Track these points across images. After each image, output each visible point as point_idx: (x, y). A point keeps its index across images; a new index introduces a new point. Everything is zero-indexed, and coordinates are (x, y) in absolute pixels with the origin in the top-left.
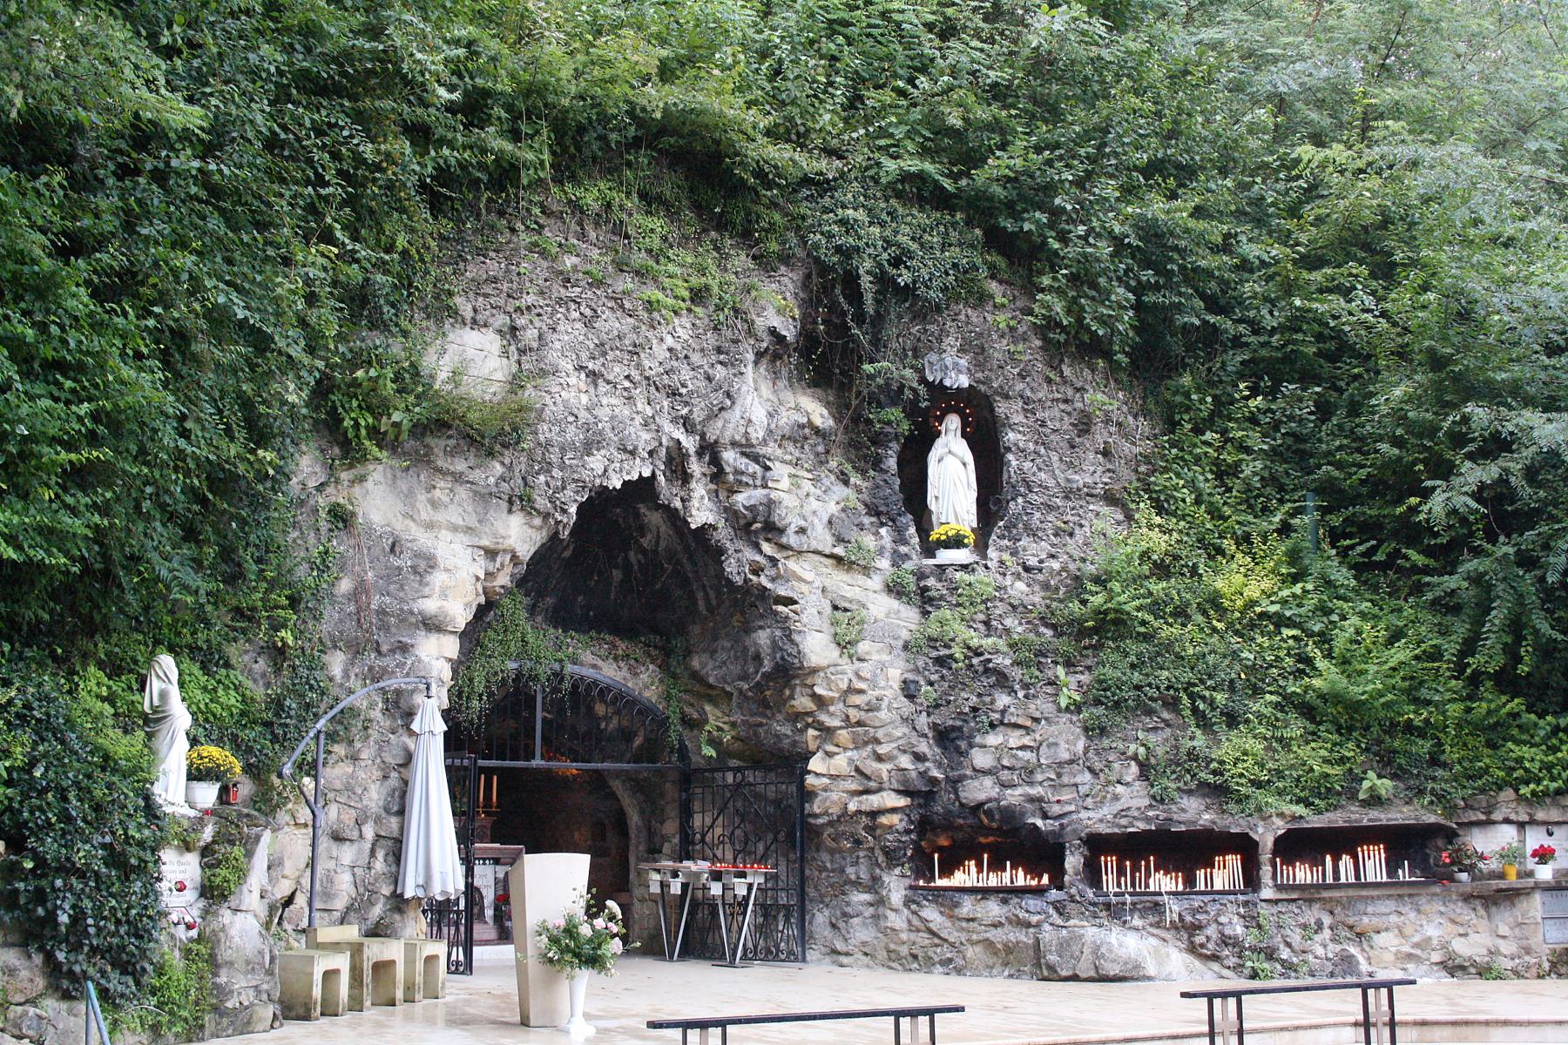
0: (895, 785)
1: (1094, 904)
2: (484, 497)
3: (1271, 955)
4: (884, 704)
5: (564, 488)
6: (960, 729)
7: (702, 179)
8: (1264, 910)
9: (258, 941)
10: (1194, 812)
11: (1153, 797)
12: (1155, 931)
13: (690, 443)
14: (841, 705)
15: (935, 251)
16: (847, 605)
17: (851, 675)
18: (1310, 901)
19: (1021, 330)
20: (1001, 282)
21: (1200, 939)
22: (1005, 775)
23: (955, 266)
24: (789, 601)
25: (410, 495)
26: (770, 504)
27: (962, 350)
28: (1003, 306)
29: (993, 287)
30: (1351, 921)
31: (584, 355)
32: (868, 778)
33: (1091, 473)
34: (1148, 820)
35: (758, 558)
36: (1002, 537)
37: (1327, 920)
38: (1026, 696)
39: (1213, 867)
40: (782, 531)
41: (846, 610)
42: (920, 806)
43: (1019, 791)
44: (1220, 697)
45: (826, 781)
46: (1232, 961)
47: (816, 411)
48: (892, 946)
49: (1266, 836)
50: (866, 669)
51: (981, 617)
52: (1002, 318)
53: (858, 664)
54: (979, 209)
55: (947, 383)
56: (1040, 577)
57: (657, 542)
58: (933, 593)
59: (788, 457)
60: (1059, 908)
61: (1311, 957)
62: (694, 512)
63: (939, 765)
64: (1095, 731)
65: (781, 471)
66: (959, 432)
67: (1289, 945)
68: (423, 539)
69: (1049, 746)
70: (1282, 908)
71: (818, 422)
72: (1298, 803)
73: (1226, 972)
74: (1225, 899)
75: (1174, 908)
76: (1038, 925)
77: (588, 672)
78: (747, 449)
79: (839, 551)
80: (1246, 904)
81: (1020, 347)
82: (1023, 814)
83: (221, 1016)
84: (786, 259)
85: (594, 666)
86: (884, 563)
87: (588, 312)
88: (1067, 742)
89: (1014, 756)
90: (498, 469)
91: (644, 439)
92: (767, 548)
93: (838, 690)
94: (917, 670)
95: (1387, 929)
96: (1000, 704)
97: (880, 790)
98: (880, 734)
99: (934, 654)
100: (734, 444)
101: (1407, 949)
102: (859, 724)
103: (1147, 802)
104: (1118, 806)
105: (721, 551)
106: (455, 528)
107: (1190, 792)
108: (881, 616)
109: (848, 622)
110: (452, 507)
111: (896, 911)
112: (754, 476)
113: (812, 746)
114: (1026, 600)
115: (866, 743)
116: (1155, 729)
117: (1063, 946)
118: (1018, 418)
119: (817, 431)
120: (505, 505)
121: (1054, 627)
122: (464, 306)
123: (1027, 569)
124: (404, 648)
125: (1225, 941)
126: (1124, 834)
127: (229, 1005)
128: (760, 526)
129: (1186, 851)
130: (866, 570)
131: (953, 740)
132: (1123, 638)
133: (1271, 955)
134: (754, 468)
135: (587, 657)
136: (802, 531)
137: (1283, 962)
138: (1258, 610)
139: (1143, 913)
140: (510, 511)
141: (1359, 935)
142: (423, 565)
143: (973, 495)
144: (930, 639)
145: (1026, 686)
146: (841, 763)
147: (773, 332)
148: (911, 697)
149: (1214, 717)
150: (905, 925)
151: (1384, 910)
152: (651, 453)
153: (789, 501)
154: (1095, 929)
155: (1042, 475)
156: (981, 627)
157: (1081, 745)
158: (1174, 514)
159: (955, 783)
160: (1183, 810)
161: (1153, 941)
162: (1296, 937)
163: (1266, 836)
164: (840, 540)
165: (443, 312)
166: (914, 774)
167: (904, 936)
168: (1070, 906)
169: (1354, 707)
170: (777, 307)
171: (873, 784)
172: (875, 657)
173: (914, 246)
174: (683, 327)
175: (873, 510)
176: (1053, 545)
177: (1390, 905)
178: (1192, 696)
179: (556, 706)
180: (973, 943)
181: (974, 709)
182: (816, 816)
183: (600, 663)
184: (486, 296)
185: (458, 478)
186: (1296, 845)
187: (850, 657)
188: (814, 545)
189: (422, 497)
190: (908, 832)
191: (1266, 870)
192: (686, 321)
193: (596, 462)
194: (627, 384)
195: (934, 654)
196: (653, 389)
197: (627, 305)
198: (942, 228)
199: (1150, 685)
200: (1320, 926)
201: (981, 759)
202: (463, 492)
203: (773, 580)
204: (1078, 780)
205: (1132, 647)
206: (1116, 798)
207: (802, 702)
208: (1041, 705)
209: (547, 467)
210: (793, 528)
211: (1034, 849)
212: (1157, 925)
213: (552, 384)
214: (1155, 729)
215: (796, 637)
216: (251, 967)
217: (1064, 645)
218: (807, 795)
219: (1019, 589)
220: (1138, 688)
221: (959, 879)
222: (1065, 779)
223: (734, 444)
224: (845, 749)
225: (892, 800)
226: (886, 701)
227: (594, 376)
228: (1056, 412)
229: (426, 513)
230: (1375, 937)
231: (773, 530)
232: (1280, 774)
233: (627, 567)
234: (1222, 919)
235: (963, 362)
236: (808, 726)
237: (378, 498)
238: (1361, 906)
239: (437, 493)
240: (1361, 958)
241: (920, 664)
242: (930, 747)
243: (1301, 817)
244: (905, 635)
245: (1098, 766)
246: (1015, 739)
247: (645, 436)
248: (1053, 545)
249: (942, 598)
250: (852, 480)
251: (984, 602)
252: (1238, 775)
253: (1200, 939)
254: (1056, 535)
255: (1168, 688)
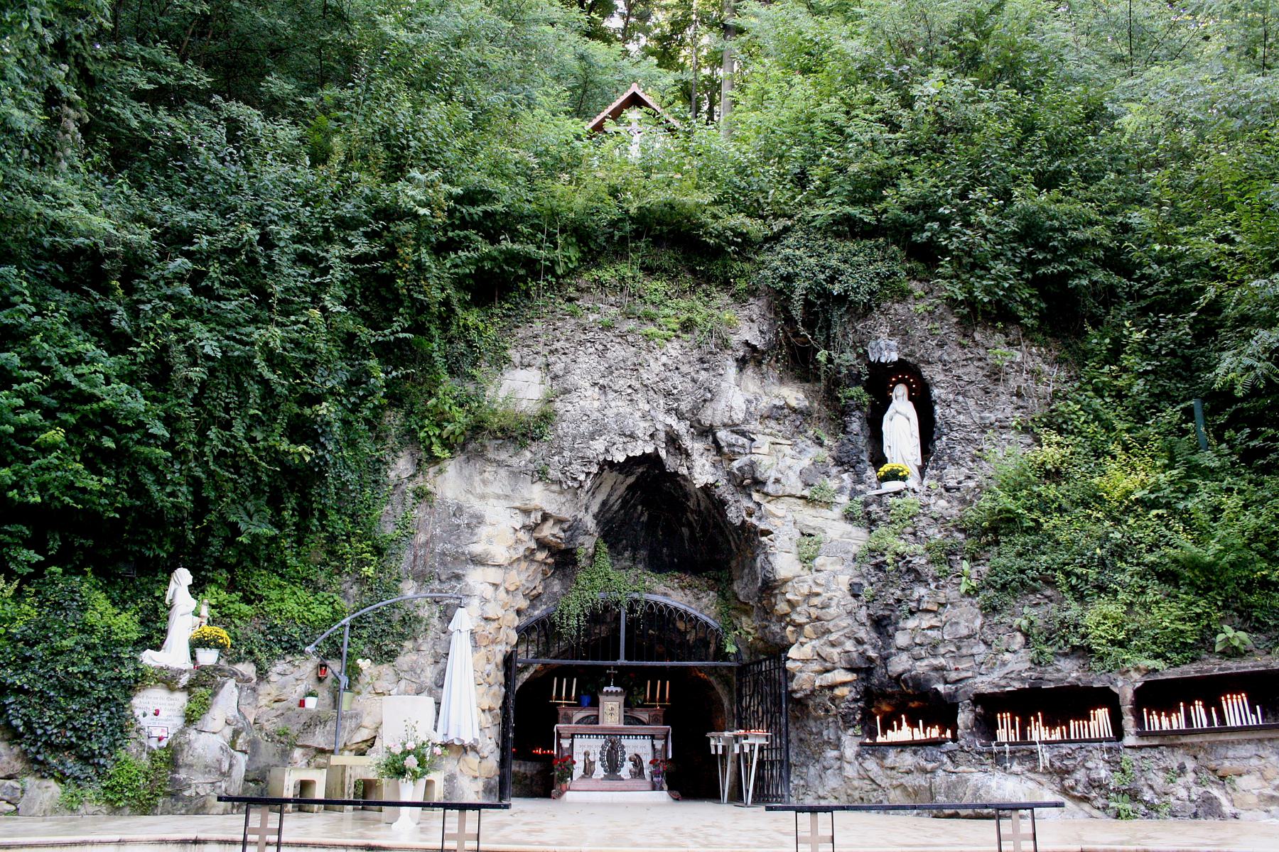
0: (844, 665)
1: (980, 753)
2: (515, 474)
3: (1134, 796)
4: (833, 603)
5: (570, 463)
6: (889, 617)
7: (678, 246)
8: (1128, 756)
9: (218, 754)
10: (1069, 672)
11: (1032, 661)
12: (1032, 776)
13: (681, 427)
14: (806, 606)
15: (857, 268)
16: (812, 532)
17: (811, 583)
18: (1172, 747)
19: (938, 312)
20: (920, 281)
21: (1069, 782)
22: (916, 650)
23: (878, 274)
24: (766, 533)
25: (470, 479)
26: (752, 465)
27: (891, 334)
28: (921, 297)
29: (914, 285)
30: (1213, 765)
31: (596, 376)
32: (825, 660)
33: (1005, 409)
34: (1023, 680)
35: (751, 505)
36: (932, 468)
37: (1190, 764)
38: (937, 587)
39: (1089, 720)
40: (764, 483)
41: (810, 535)
42: (863, 680)
43: (925, 662)
44: (1092, 573)
45: (799, 664)
46: (1100, 802)
47: (794, 395)
48: (849, 791)
49: (1126, 689)
50: (821, 578)
51: (910, 530)
52: (920, 307)
53: (816, 574)
54: (898, 232)
55: (883, 360)
56: (958, 494)
57: (699, 505)
58: (873, 516)
59: (767, 431)
60: (951, 756)
61: (1172, 799)
62: (696, 476)
63: (875, 647)
64: (990, 609)
65: (763, 442)
66: (906, 397)
67: (1151, 787)
68: (477, 506)
69: (951, 625)
70: (1144, 753)
71: (794, 403)
72: (1156, 658)
73: (1095, 813)
74: (1090, 746)
75: (1045, 756)
76: (933, 771)
77: (661, 599)
78: (734, 428)
79: (806, 493)
80: (1109, 750)
81: (937, 325)
82: (928, 681)
83: (177, 800)
84: (753, 292)
85: (665, 594)
86: (844, 499)
87: (601, 347)
88: (967, 621)
89: (925, 635)
90: (528, 455)
91: (642, 428)
92: (756, 496)
93: (802, 595)
94: (862, 575)
95: (1248, 772)
96: (916, 596)
97: (834, 669)
98: (830, 626)
99: (874, 561)
100: (725, 425)
101: (1269, 791)
102: (818, 619)
103: (1028, 665)
104: (1006, 670)
105: (723, 503)
106: (498, 497)
107: (1066, 655)
108: (836, 537)
109: (812, 546)
110: (496, 483)
111: (849, 763)
112: (743, 446)
113: (791, 638)
114: (945, 513)
115: (824, 633)
116: (1038, 604)
117: (951, 788)
118: (938, 378)
119: (794, 410)
120: (529, 478)
121: (963, 531)
122: (514, 355)
123: (948, 490)
124: (458, 577)
125: (1094, 784)
126: (1002, 693)
127: (187, 793)
128: (750, 482)
129: (1065, 705)
130: (828, 505)
131: (885, 626)
132: (1013, 532)
133: (1134, 796)
134: (742, 440)
135: (661, 588)
136: (777, 481)
137: (1146, 803)
138: (1133, 497)
139: (1022, 761)
140: (533, 483)
141: (1222, 778)
142: (474, 521)
143: (918, 441)
144: (870, 550)
145: (936, 579)
146: (807, 651)
147: (747, 343)
148: (855, 596)
149: (1087, 589)
150: (856, 775)
151: (1244, 754)
152: (652, 436)
153: (766, 461)
154: (981, 775)
155: (962, 417)
156: (911, 538)
157: (978, 622)
158: (1072, 433)
159: (885, 659)
160: (1058, 671)
161: (1031, 784)
162: (1159, 780)
163: (1126, 689)
164: (807, 485)
165: (501, 361)
166: (855, 655)
167: (856, 783)
168: (960, 755)
169: (1208, 569)
170: (749, 327)
171: (828, 665)
172: (829, 568)
173: (842, 266)
174: (674, 349)
175: (839, 462)
176: (970, 469)
177: (1251, 749)
178: (1068, 574)
179: (631, 625)
180: (895, 788)
181: (899, 601)
182: (794, 691)
183: (670, 592)
184: (528, 346)
185: (499, 464)
186: (1157, 696)
187: (810, 569)
188: (788, 490)
189: (477, 478)
190: (855, 700)
191: (1129, 722)
192: (676, 344)
193: (599, 445)
194: (630, 391)
195: (875, 560)
196: (651, 393)
197: (630, 339)
198: (868, 251)
199: (1032, 568)
200: (1182, 769)
201: (901, 639)
202: (503, 472)
203: (760, 519)
204: (974, 651)
205: (1020, 539)
206: (1004, 664)
207: (782, 607)
208: (950, 593)
209: (560, 451)
210: (772, 479)
211: (936, 709)
212: (1033, 770)
213: (573, 397)
214: (1038, 604)
215: (771, 558)
216: (207, 769)
217: (969, 544)
218: (789, 676)
219: (940, 505)
220: (1022, 571)
221: (893, 736)
222: (964, 651)
223: (725, 425)
224: (811, 639)
225: (841, 676)
226: (836, 600)
227: (603, 387)
228: (971, 369)
229: (479, 489)
230: (1238, 780)
231: (758, 483)
232: (1136, 632)
233: (689, 525)
234: (1090, 764)
235: (894, 343)
236: (788, 624)
237: (451, 482)
238: (1222, 751)
239: (486, 475)
240: (1224, 800)
241: (864, 570)
242: (868, 633)
243: (1155, 670)
244: (854, 549)
245: (989, 638)
246: (927, 621)
247: (643, 424)
248: (970, 469)
249: (880, 519)
250: (826, 442)
251: (910, 518)
252: (1098, 635)
253: (1069, 782)
254: (973, 461)
255: (1047, 569)
